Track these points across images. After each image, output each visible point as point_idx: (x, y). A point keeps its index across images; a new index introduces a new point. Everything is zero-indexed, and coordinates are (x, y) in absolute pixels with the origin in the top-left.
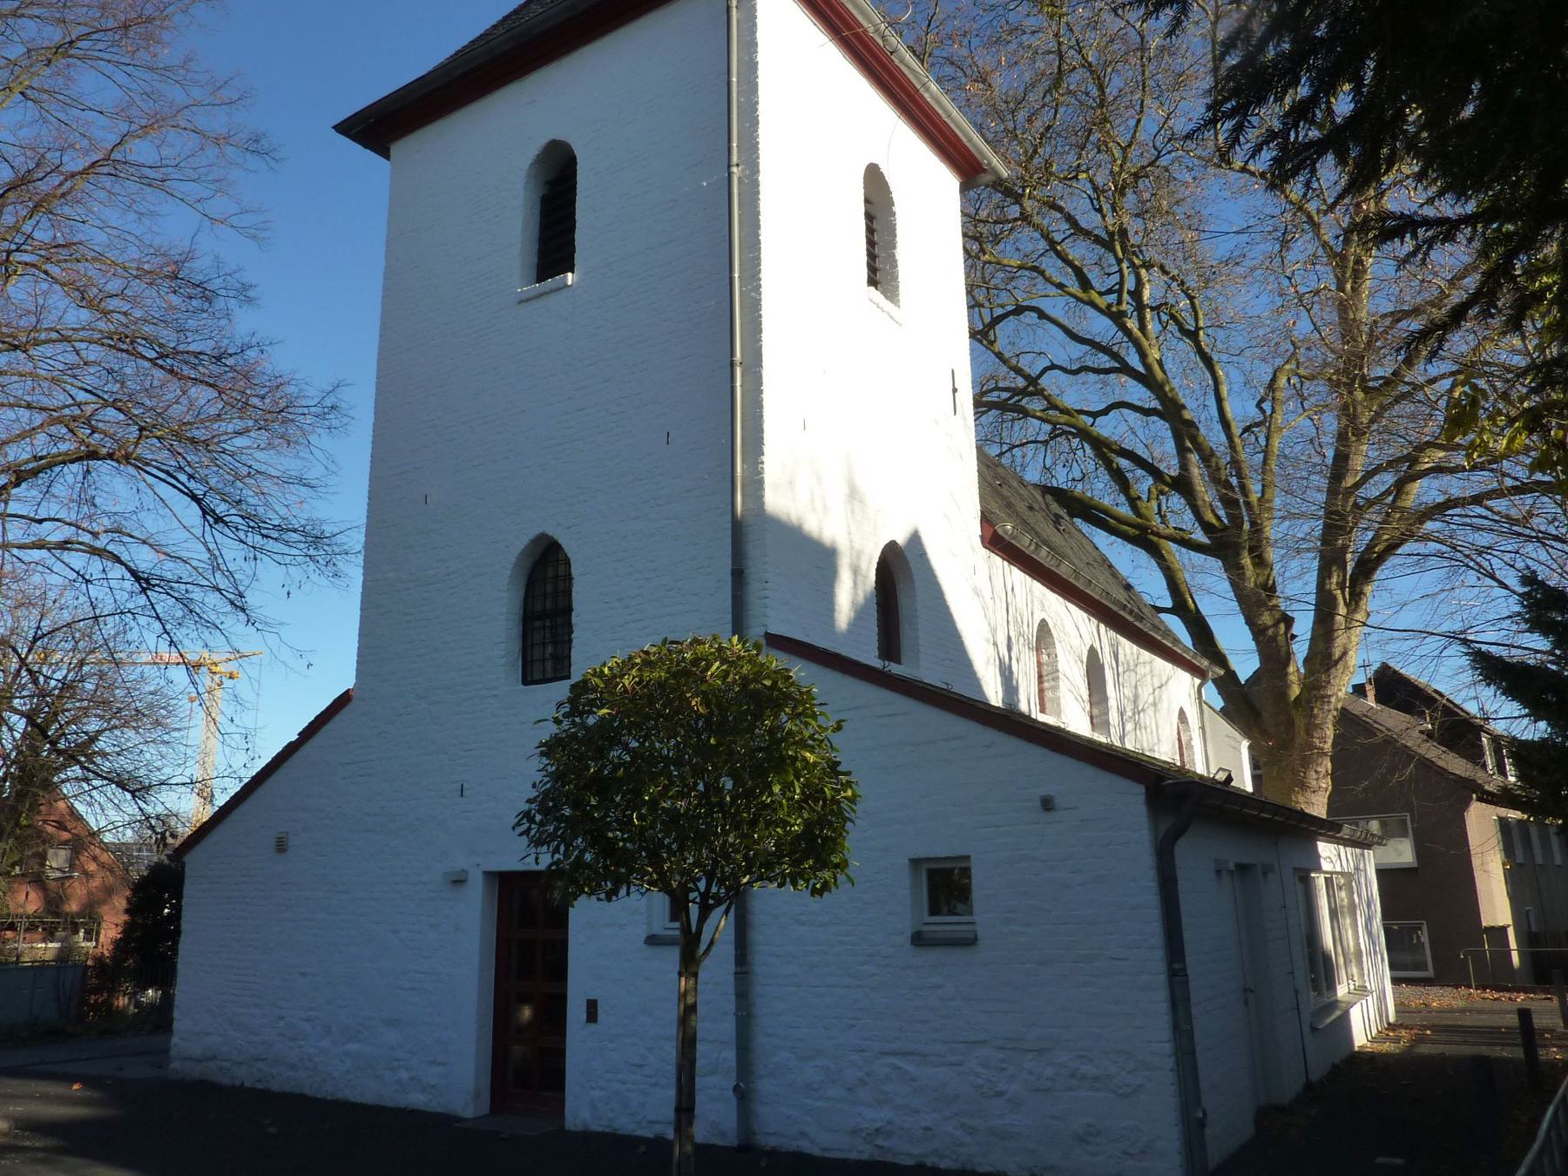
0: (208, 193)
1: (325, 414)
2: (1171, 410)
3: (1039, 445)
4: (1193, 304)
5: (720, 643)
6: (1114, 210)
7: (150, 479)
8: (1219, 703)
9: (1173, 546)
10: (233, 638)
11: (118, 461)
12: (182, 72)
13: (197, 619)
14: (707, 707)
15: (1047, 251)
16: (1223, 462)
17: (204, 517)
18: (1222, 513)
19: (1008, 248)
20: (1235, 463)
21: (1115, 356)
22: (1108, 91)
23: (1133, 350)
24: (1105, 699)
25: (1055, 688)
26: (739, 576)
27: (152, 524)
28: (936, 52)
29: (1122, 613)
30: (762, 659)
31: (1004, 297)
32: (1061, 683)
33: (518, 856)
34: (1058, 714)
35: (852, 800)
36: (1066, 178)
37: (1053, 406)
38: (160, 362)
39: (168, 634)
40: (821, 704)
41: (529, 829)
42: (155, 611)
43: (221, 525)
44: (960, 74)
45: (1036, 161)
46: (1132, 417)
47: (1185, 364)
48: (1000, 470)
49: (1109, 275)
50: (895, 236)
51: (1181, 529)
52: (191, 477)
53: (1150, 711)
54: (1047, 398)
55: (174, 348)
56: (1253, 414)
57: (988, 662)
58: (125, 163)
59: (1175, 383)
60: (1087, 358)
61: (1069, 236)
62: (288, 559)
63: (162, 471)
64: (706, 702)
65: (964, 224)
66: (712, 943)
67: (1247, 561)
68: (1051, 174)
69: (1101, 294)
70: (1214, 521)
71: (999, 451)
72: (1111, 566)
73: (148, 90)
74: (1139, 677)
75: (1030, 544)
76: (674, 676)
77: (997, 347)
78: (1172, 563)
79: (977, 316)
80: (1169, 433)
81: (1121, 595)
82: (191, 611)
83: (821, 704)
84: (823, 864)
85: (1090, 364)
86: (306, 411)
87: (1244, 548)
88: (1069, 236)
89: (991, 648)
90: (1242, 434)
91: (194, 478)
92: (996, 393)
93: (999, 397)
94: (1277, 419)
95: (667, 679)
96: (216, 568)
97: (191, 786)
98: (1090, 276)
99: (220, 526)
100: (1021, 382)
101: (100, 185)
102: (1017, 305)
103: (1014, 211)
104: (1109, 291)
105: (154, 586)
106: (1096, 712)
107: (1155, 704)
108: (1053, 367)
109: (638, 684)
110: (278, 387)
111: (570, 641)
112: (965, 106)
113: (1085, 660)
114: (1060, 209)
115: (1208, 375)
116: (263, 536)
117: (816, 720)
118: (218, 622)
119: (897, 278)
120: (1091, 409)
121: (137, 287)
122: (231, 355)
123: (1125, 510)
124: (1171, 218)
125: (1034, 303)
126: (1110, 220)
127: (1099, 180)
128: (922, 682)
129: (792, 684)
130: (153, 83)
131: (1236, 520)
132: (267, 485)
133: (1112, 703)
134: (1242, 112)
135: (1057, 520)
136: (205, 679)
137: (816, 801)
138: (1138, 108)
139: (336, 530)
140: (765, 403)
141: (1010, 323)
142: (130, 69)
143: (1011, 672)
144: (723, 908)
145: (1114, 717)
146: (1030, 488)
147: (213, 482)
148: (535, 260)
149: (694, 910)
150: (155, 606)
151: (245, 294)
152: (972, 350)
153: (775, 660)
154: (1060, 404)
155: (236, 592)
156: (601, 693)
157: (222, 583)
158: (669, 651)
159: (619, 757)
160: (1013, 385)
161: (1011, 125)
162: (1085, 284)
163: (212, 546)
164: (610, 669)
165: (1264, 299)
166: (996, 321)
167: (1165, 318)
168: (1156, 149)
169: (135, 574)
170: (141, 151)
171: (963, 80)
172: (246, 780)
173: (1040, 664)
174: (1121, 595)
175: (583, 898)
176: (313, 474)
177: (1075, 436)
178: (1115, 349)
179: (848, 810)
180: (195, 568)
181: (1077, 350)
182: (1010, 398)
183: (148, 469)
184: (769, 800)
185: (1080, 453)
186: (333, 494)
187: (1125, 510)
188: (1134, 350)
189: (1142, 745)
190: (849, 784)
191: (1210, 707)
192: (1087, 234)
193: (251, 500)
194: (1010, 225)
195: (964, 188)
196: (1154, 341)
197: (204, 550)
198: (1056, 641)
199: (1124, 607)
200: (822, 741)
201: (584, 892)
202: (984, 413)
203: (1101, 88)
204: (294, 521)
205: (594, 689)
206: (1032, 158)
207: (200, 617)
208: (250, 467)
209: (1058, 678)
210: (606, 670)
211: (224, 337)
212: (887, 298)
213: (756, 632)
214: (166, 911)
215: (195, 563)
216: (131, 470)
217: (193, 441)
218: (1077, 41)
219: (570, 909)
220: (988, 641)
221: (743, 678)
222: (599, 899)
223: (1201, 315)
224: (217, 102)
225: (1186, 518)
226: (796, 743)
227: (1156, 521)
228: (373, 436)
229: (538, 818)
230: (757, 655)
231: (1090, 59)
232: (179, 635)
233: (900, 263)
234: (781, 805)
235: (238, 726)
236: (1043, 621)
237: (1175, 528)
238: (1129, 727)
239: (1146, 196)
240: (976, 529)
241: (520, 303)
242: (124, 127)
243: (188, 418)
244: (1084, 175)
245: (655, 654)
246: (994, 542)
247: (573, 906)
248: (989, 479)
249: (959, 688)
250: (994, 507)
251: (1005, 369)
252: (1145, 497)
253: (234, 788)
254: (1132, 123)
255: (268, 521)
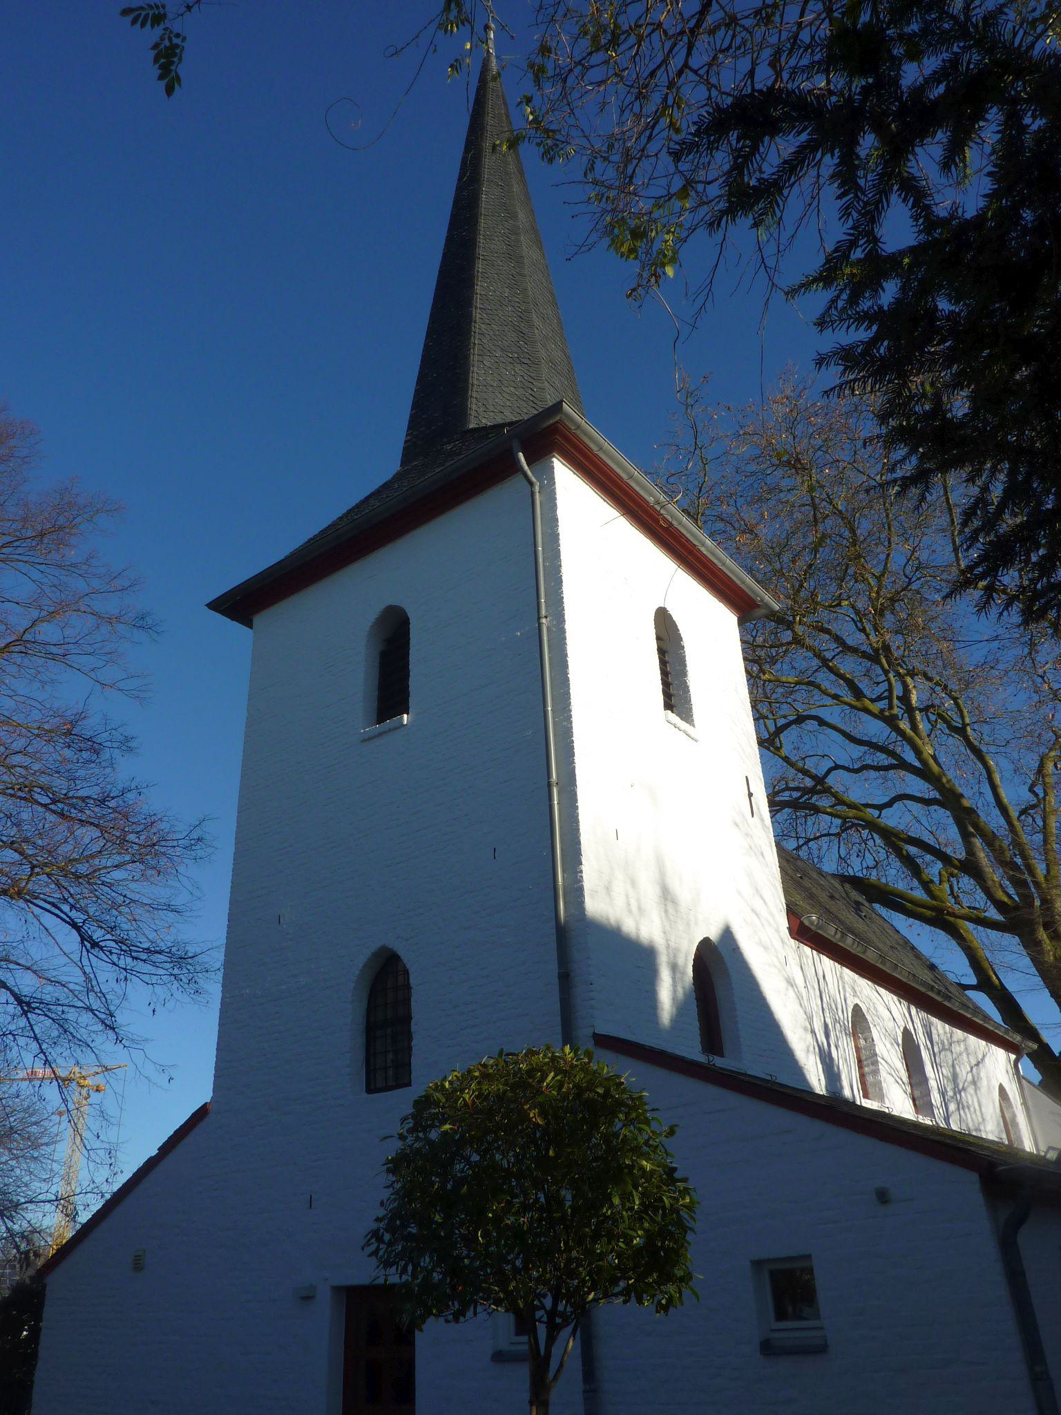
0: (101, 664)
1: (192, 845)
2: (950, 799)
3: (832, 837)
4: (957, 704)
5: (553, 1053)
6: (876, 630)
7: (37, 911)
8: (1036, 1076)
9: (970, 926)
10: (102, 1056)
11: (12, 898)
12: (84, 567)
13: (71, 1038)
14: (545, 1119)
15: (820, 667)
16: (1006, 843)
17: (82, 943)
18: (1012, 891)
19: (785, 667)
20: (1017, 844)
21: (892, 754)
22: (858, 532)
23: (907, 748)
24: (926, 1080)
25: (876, 1072)
26: (565, 977)
27: (37, 952)
28: (707, 512)
29: (930, 993)
30: (593, 1066)
31: (785, 709)
32: (880, 1067)
33: (365, 1271)
34: (881, 1097)
35: (690, 1208)
36: (831, 606)
37: (841, 802)
38: (52, 807)
39: (44, 1054)
40: (653, 1110)
41: (378, 1250)
42: (34, 1032)
43: (97, 949)
44: (729, 528)
45: (802, 594)
46: (916, 807)
47: (957, 757)
48: (799, 863)
49: (878, 683)
50: (685, 666)
51: (974, 908)
52: (72, 907)
53: (971, 1090)
54: (835, 795)
55: (65, 795)
56: (1028, 798)
57: (808, 1051)
58: (34, 642)
59: (951, 774)
60: (867, 758)
61: (838, 654)
62: (154, 979)
63: (49, 903)
64: (543, 1114)
65: (743, 650)
66: (561, 1365)
67: (1042, 934)
68: (817, 603)
69: (873, 701)
70: (1006, 899)
71: (796, 845)
72: (913, 948)
73: (56, 582)
74: (954, 1056)
75: (836, 933)
76: (514, 1087)
77: (784, 752)
78: (971, 942)
79: (762, 727)
80: (951, 820)
81: (926, 976)
82: (66, 1031)
83: (653, 1110)
84: (667, 1277)
85: (869, 762)
86: (175, 843)
87: (1038, 923)
88: (838, 654)
89: (809, 1036)
90: (1020, 816)
91: (75, 908)
92: (787, 793)
93: (791, 796)
94: (1050, 802)
95: (505, 1092)
96: (90, 990)
97: (56, 1203)
98: (860, 686)
99: (96, 951)
100: (809, 783)
101: (12, 661)
102: (797, 715)
103: (787, 636)
104: (879, 699)
105: (34, 1009)
106: (917, 1094)
107: (974, 1082)
108: (837, 767)
109: (477, 1097)
110: (152, 823)
111: (410, 1048)
112: (736, 554)
113: (900, 1042)
114: (828, 632)
115: (980, 765)
116: (134, 958)
117: (649, 1126)
118: (89, 1040)
119: (690, 701)
120: (875, 803)
121: (38, 744)
122: (113, 798)
123: (919, 894)
124: (926, 632)
125: (813, 712)
126: (873, 638)
127: (860, 605)
128: (746, 1075)
129: (624, 1091)
130: (61, 577)
131: (1027, 899)
132: (139, 911)
133: (933, 1084)
134: (992, 572)
135: (858, 906)
136: (75, 1095)
137: (656, 1210)
138: (886, 543)
139: (199, 951)
140: (581, 818)
141: (793, 732)
142: (42, 567)
143: (831, 1059)
144: (569, 1329)
145: (936, 1098)
146: (829, 878)
147: (91, 911)
148: (375, 705)
149: (542, 1330)
150: (35, 1027)
151: (126, 745)
152: (761, 756)
153: (607, 1064)
154: (845, 798)
155: (107, 1012)
156: (443, 1107)
157: (96, 1004)
158: (506, 1062)
159: (462, 1171)
160: (802, 786)
161: (778, 566)
162: (858, 693)
163: (88, 969)
164: (451, 1083)
165: (1023, 696)
166: (780, 730)
167: (933, 718)
168: (906, 577)
169: (19, 999)
170: (48, 632)
171: (733, 533)
172: (108, 1196)
173: (858, 1049)
174: (926, 976)
175: (431, 1320)
176: (177, 902)
177: (864, 828)
178: (891, 747)
179: (688, 1219)
180: (71, 991)
181: (857, 751)
182: (801, 797)
183: (35, 901)
184: (609, 1212)
185: (870, 843)
186: (197, 917)
187: (919, 894)
188: (909, 747)
189: (967, 1125)
190: (686, 1191)
191: (1029, 1082)
192: (854, 650)
193: (125, 926)
194: (784, 648)
195: (741, 623)
196: (927, 740)
197: (80, 973)
198: (871, 1026)
199: (932, 988)
200: (656, 1147)
201: (432, 1314)
202: (778, 811)
203: (853, 531)
204: (162, 944)
205: (437, 1104)
206: (798, 591)
207: (74, 1037)
208: (125, 896)
209: (877, 1062)
210: (447, 1085)
211: (108, 783)
212: (682, 719)
213: (584, 1033)
214: (25, 1333)
215: (71, 986)
216: (21, 903)
217: (77, 877)
218: (827, 494)
219: (417, 1332)
220: (805, 1029)
221: (577, 1086)
222: (447, 1321)
223: (965, 712)
224: (112, 589)
225: (978, 898)
226: (632, 1150)
227: (950, 902)
228: (234, 864)
229: (387, 1237)
230: (589, 1063)
231: (840, 508)
232: (53, 1053)
233: (691, 689)
234: (622, 1217)
235: (103, 1141)
236: (856, 1006)
237: (969, 907)
238: (952, 1107)
239: (903, 615)
240: (783, 923)
241: (362, 742)
242: (35, 614)
243: (75, 856)
244: (846, 603)
245: (492, 1066)
246: (801, 932)
247: (421, 1330)
248: (790, 872)
249: (784, 1079)
250: (798, 898)
251: (793, 771)
252: (936, 880)
253: (96, 1205)
254: (883, 557)
255: (138, 944)
